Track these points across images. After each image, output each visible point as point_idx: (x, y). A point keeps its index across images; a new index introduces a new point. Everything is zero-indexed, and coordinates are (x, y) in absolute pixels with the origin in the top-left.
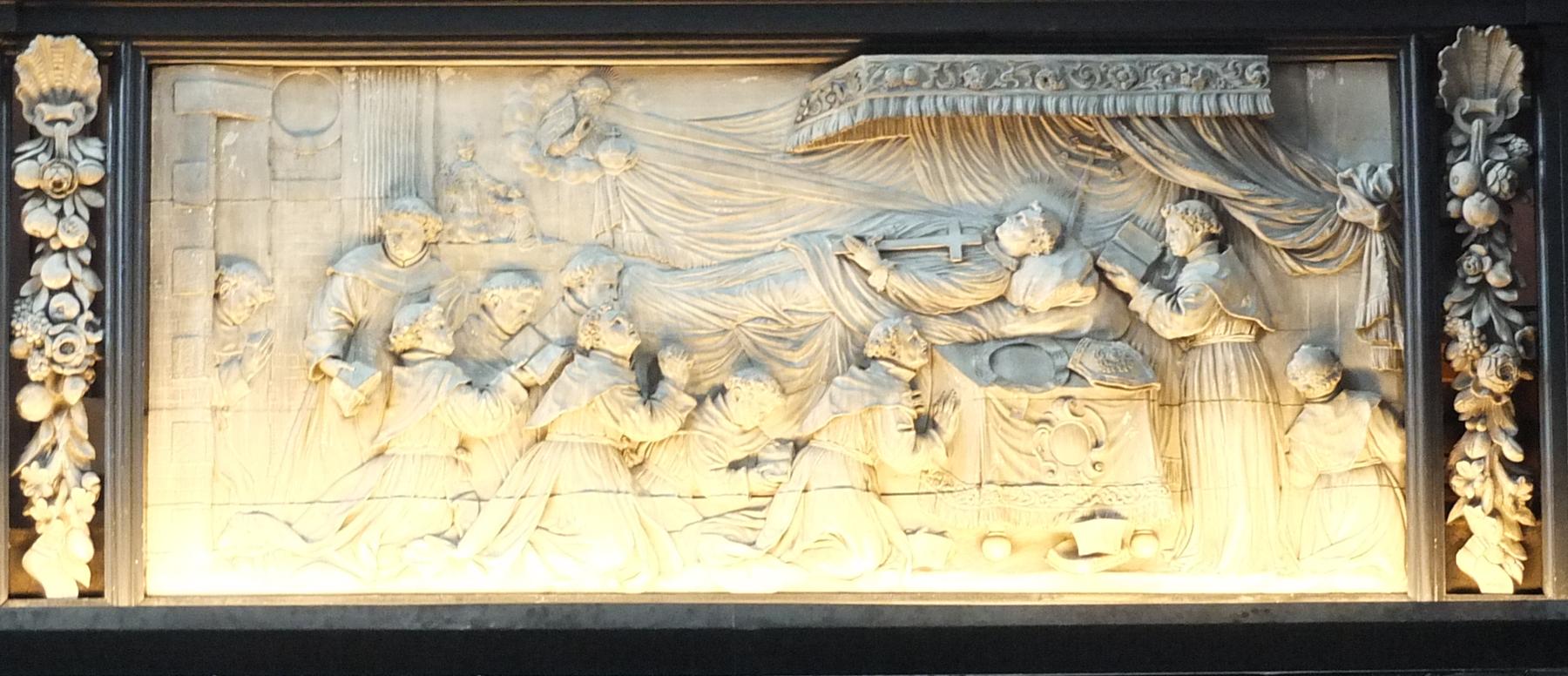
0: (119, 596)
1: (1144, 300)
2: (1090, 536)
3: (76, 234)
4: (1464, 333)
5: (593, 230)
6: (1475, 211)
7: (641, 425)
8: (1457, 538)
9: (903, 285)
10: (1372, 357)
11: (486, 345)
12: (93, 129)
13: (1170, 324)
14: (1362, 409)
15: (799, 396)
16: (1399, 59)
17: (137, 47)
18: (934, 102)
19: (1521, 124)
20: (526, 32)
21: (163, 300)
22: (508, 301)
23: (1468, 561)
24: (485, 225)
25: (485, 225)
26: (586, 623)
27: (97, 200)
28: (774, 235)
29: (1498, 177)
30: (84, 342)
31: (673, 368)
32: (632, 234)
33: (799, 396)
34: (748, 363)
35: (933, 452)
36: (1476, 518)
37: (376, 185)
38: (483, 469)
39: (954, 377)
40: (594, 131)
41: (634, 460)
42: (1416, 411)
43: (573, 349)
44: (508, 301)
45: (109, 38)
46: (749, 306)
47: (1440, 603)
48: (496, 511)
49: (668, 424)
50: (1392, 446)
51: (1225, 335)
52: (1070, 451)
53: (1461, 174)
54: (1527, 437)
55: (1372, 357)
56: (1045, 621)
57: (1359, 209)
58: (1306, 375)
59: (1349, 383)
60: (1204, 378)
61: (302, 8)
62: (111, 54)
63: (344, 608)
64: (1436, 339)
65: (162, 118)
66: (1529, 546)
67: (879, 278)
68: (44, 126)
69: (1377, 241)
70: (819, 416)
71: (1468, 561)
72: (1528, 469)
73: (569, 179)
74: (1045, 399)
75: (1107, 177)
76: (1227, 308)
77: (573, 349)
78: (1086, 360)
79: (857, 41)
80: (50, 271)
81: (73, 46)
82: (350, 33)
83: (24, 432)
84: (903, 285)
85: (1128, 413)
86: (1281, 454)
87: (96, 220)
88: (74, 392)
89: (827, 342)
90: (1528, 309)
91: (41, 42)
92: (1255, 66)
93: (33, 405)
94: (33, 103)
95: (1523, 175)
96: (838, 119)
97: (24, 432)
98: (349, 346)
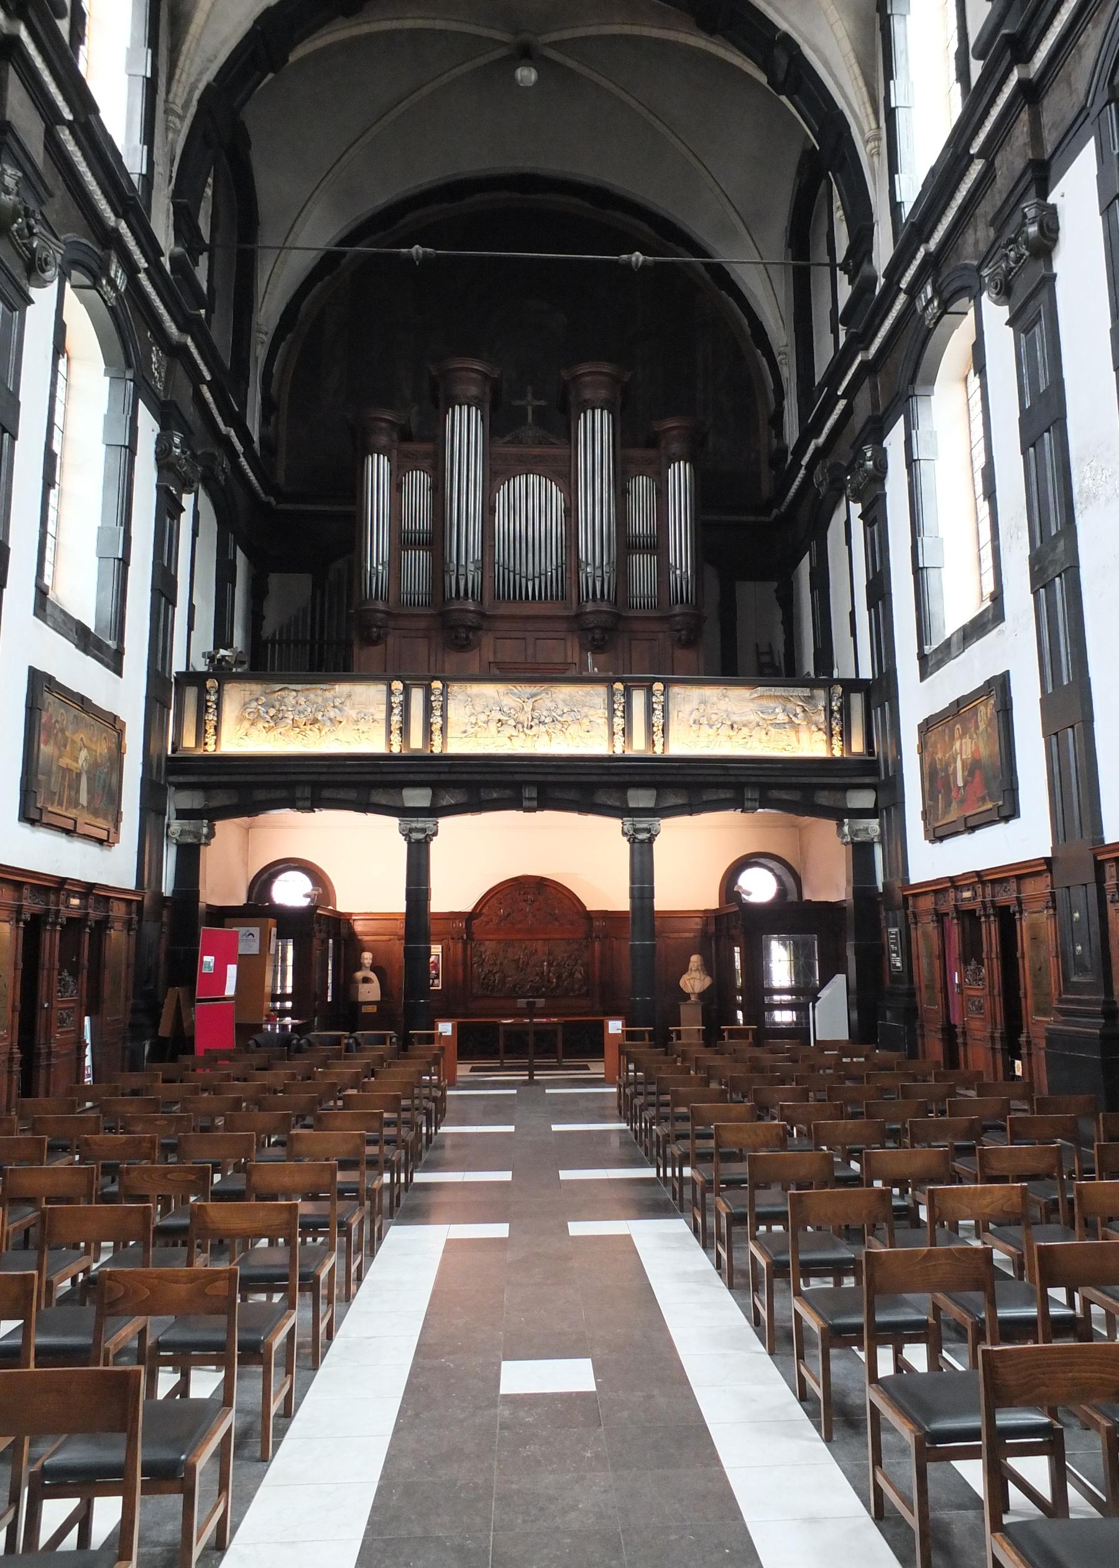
0: (444, 752)
1: (794, 719)
2: (787, 748)
3: (621, 708)
4: (834, 723)
5: (725, 709)
6: (835, 708)
7: (731, 733)
8: (833, 749)
9: (764, 716)
10: (822, 727)
11: (712, 723)
12: (662, 695)
13: (797, 721)
14: (821, 733)
15: (751, 730)
18: (768, 693)
19: (841, 698)
21: (671, 716)
22: (714, 717)
23: (834, 752)
24: (711, 707)
25: (711, 707)
28: (747, 710)
29: (839, 704)
30: (662, 721)
31: (735, 726)
32: (729, 709)
33: (751, 730)
34: (744, 726)
35: (768, 737)
36: (835, 747)
37: (697, 702)
38: (711, 738)
39: (770, 728)
40: (725, 696)
41: (730, 737)
42: (828, 733)
43: (722, 723)
44: (714, 717)
46: (744, 719)
48: (713, 743)
49: (735, 733)
50: (825, 737)
51: (804, 723)
52: (785, 737)
53: (834, 704)
54: (842, 737)
55: (822, 727)
57: (821, 708)
58: (814, 728)
59: (820, 729)
60: (801, 728)
64: (831, 724)
65: (670, 693)
66: (842, 750)
67: (761, 715)
69: (823, 712)
70: (754, 733)
71: (834, 752)
72: (842, 741)
73: (722, 702)
74: (782, 731)
75: (156, 1025)
76: (805, 720)
77: (722, 723)
78: (787, 726)
80: (657, 712)
83: (654, 733)
84: (764, 716)
85: (1017, 1463)
86: (811, 738)
87: (624, 707)
88: (661, 728)
89: (754, 723)
90: (842, 720)
92: (808, 690)
93: (655, 729)
95: (841, 704)
96: (756, 695)
97: (654, 733)
98: (694, 722)
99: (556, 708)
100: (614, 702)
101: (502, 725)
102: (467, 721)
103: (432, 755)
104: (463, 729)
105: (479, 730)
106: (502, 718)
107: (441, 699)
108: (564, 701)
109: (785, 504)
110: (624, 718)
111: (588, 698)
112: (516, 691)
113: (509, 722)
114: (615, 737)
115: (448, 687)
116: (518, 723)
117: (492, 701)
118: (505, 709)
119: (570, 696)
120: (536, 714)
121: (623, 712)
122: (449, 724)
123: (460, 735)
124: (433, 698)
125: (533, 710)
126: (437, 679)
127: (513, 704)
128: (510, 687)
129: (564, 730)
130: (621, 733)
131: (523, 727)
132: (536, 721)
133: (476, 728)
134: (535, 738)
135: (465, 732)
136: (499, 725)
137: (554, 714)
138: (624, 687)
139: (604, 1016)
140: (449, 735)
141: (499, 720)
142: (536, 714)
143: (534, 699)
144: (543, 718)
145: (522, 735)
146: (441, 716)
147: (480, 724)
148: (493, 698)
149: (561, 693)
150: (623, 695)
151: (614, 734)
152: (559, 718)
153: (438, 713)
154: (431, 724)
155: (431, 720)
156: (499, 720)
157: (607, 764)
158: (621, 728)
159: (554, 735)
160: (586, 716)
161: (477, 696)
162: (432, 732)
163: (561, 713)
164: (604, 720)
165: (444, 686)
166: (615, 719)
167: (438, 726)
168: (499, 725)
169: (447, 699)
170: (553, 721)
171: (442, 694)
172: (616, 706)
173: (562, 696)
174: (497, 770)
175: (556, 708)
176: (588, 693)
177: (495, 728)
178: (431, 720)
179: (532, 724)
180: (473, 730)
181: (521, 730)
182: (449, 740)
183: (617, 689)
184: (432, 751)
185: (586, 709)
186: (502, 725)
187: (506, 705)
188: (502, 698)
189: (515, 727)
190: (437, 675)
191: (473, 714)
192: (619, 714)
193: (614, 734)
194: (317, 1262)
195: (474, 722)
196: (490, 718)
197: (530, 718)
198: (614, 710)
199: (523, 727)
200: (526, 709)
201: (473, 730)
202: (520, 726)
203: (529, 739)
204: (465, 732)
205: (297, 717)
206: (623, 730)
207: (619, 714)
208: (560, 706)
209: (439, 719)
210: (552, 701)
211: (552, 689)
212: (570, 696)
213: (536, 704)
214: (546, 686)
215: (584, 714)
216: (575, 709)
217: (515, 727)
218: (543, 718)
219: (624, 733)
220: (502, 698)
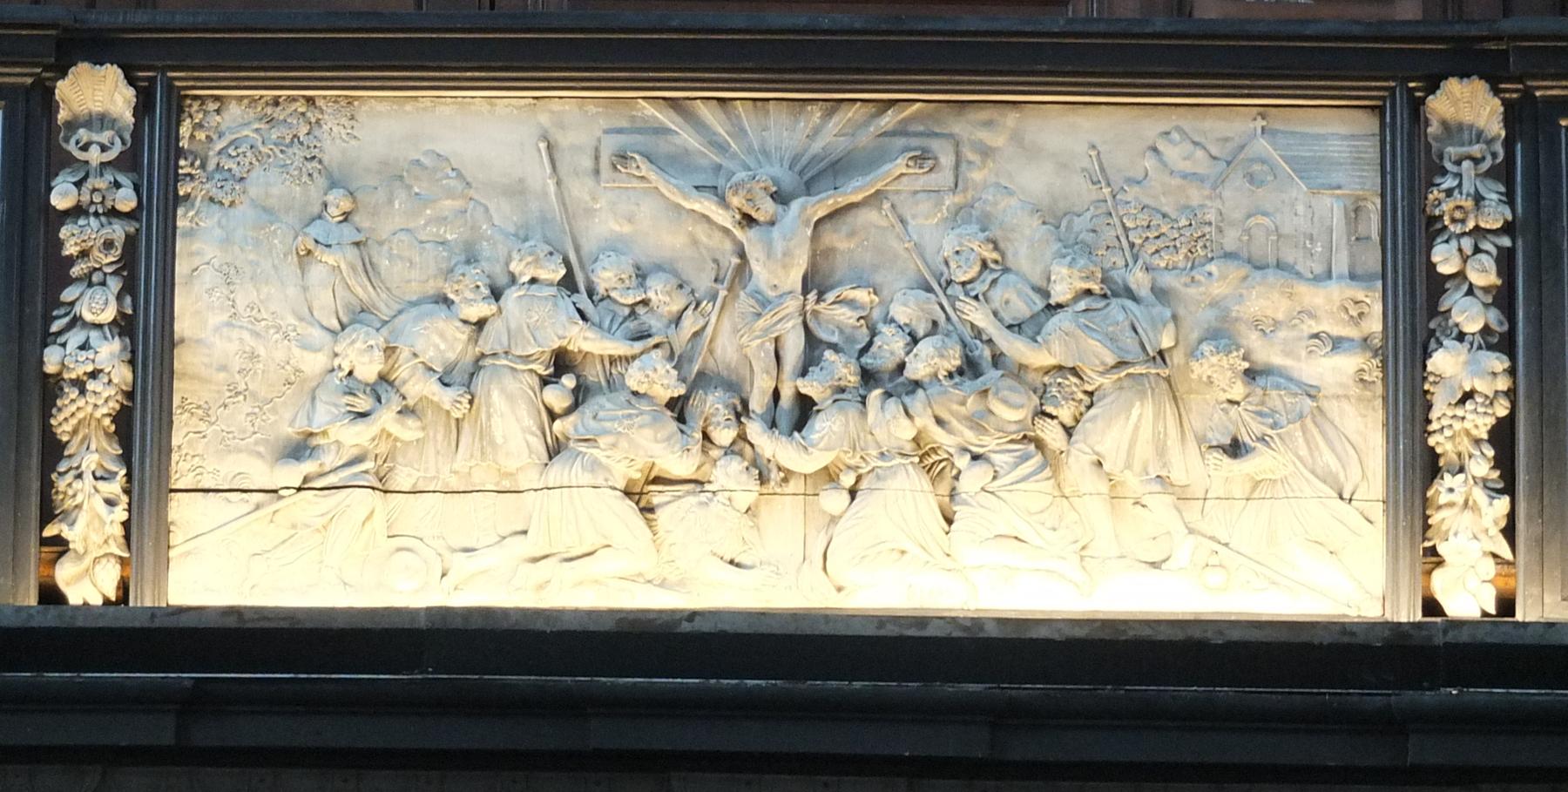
0: (143, 599)
3: (1484, 274)
16: (1385, 105)
17: (1532, 87)
20: (1006, 68)
26: (540, 625)
27: (1506, 242)
45: (149, 69)
47: (1419, 623)
56: (791, 629)
61: (1188, 45)
62: (147, 84)
63: (1268, 644)
68: (80, 152)
79: (140, 74)
81: (112, 74)
82: (531, 65)
87: (1505, 261)
91: (83, 69)
94: (72, 126)
99: (995, 267)
100: (1432, 229)
101: (580, 395)
102: (314, 363)
103: (51, 618)
104: (289, 431)
105: (408, 431)
106: (587, 341)
107: (126, 200)
108: (1054, 217)
109: (787, 685)
110: (1506, 345)
111: (1235, 197)
112: (687, 138)
113: (634, 378)
114: (1448, 488)
115: (177, 109)
116: (702, 380)
117: (504, 214)
118: (606, 277)
119: (1100, 177)
120: (838, 317)
121: (1503, 299)
122: (181, 389)
123: (262, 474)
124: (62, 196)
125: (814, 283)
126: (98, 47)
127: (668, 240)
128: (647, 108)
129: (1051, 434)
130: (1481, 466)
131: (742, 411)
132: (842, 368)
133: (386, 418)
134: (835, 500)
135: (299, 449)
136: (557, 397)
137: (978, 316)
138: (1513, 115)
139: (1483, 622)
140: (182, 472)
141: (562, 362)
142: (838, 317)
143: (831, 201)
144: (891, 346)
145: (730, 474)
146: (124, 326)
147: (420, 387)
148: (516, 190)
149: (1032, 152)
150: (1503, 173)
151: (1431, 466)
152: (1016, 348)
153: (100, 306)
154: (51, 389)
155: (52, 360)
156: (562, 362)
157: (1375, 699)
158: (1481, 424)
159: (973, 479)
160: (1221, 335)
161: (396, 176)
162: (53, 451)
163: (1021, 305)
164: (1349, 363)
165: (143, 107)
166: (1446, 362)
167: (102, 401)
168: (557, 397)
169: (173, 201)
170: (969, 368)
171: (129, 161)
172: (1445, 259)
173: (1036, 180)
174: (549, 735)
175: (995, 267)
176: (1232, 159)
177: (524, 412)
178: (52, 360)
179: (809, 387)
180: (355, 436)
181: (724, 436)
182: (181, 510)
183: (1452, 131)
184: (51, 595)
185: (1220, 282)
186: (580, 395)
187: (615, 246)
188: (580, 189)
189: (678, 408)
190: (101, 18)
191: (358, 316)
192: (1470, 316)
193: (1431, 466)
194: (1416, 138)
195: (368, 370)
196: (492, 339)
197: (794, 347)
198: (1437, 284)
199: (742, 411)
200: (761, 272)
201: (355, 436)
202: (713, 404)
203: (785, 511)
204: (299, 449)
205: (335, 129)
206: (1502, 436)
207: (1470, 316)
208: (1022, 257)
209: (109, 351)
210: (958, 216)
211: (960, 126)
212: (1100, 177)
213: (835, 238)
214: (915, 105)
215: (1199, 318)
216: (1138, 280)
217: (678, 408)
218: (891, 346)
219: (1505, 462)
220: (580, 189)
